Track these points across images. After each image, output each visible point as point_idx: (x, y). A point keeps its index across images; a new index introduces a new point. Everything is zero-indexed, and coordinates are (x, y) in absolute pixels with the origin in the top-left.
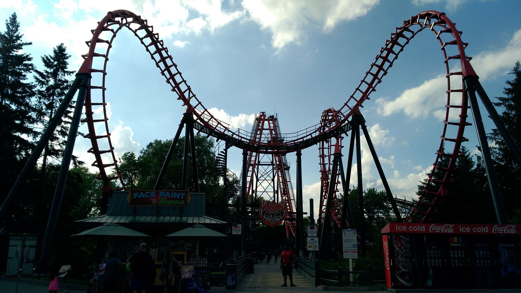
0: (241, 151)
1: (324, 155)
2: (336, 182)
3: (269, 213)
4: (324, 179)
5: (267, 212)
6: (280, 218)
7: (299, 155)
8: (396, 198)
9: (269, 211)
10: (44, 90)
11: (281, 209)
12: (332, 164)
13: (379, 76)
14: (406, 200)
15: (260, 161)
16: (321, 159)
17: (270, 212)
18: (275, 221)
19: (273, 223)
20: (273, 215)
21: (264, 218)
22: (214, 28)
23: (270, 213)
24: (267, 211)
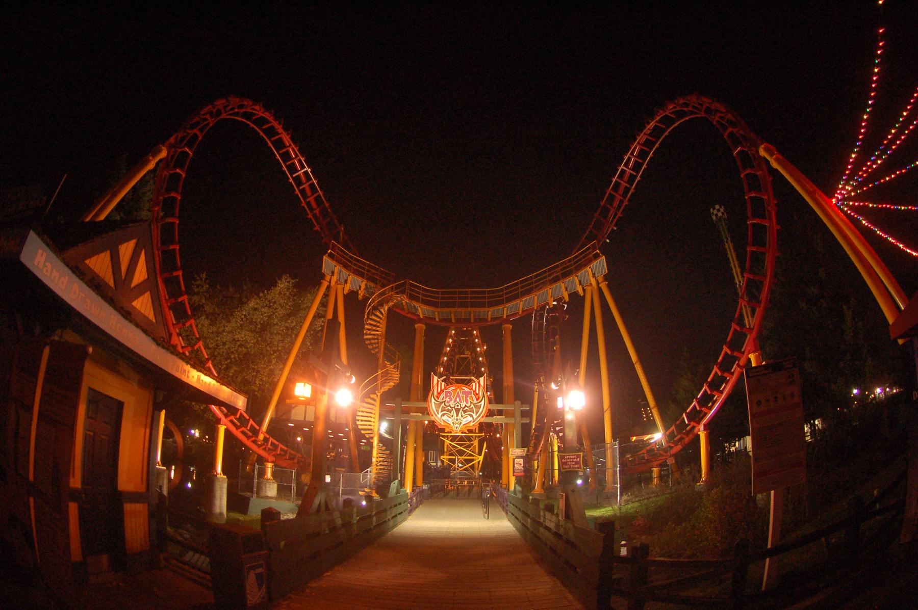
5: (445, 404)
6: (471, 416)
9: (448, 402)
10: (192, 298)
11: (474, 397)
17: (452, 404)
19: (457, 428)
20: (457, 411)
22: (260, 511)
23: (450, 407)
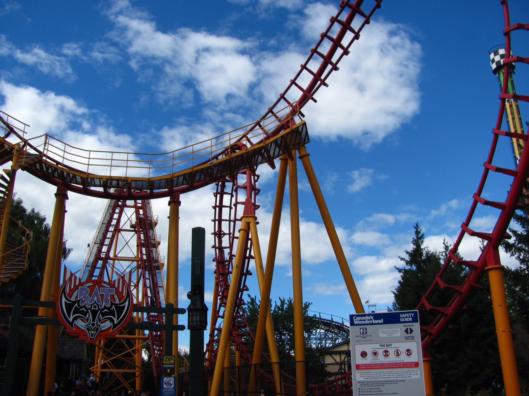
0: (54, 189)
1: (222, 233)
2: (245, 272)
3: (85, 306)
4: (220, 274)
5: (78, 305)
6: (112, 320)
7: (175, 204)
8: (320, 318)
12: (237, 238)
13: (345, 42)
14: (334, 320)
15: (118, 256)
16: (217, 238)
18: (98, 329)
19: (92, 335)
21: (71, 320)
23: (86, 309)
24: (78, 301)
